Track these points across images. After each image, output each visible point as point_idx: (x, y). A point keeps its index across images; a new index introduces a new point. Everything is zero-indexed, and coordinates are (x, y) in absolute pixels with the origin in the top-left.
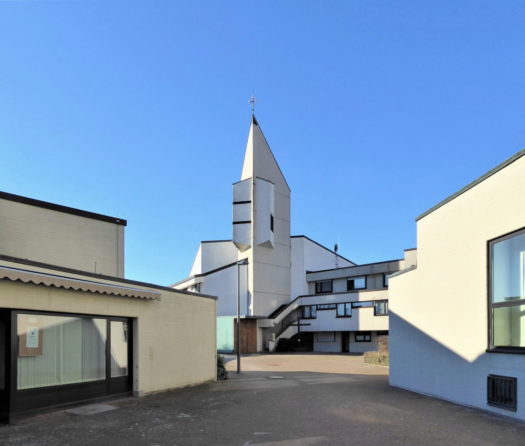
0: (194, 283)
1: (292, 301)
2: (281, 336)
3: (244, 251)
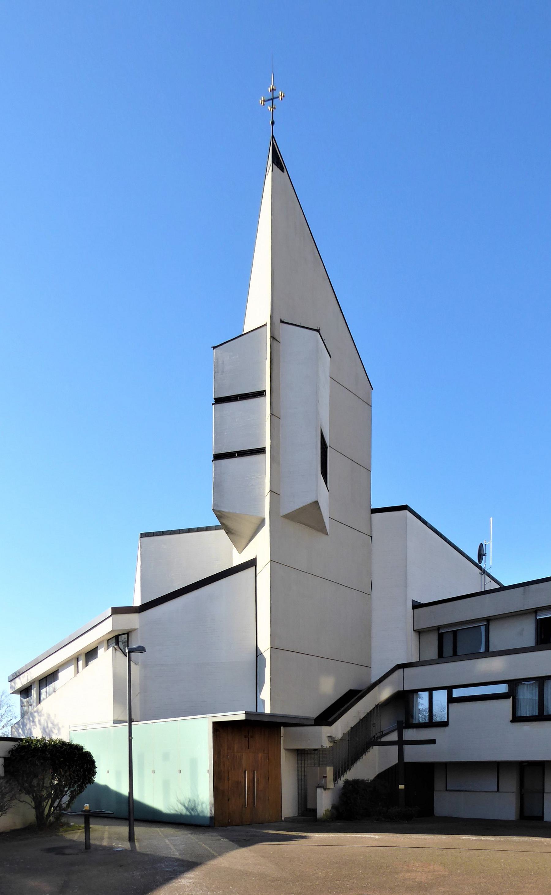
0: (111, 629)
1: (374, 680)
2: (351, 775)
3: (246, 547)
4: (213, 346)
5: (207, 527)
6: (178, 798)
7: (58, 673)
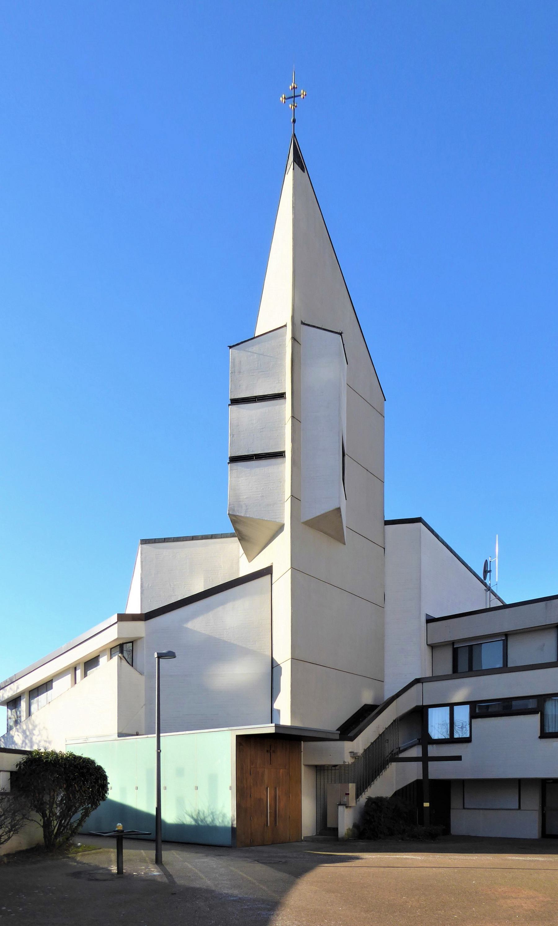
0: (116, 637)
4: (229, 345)
5: (193, 537)
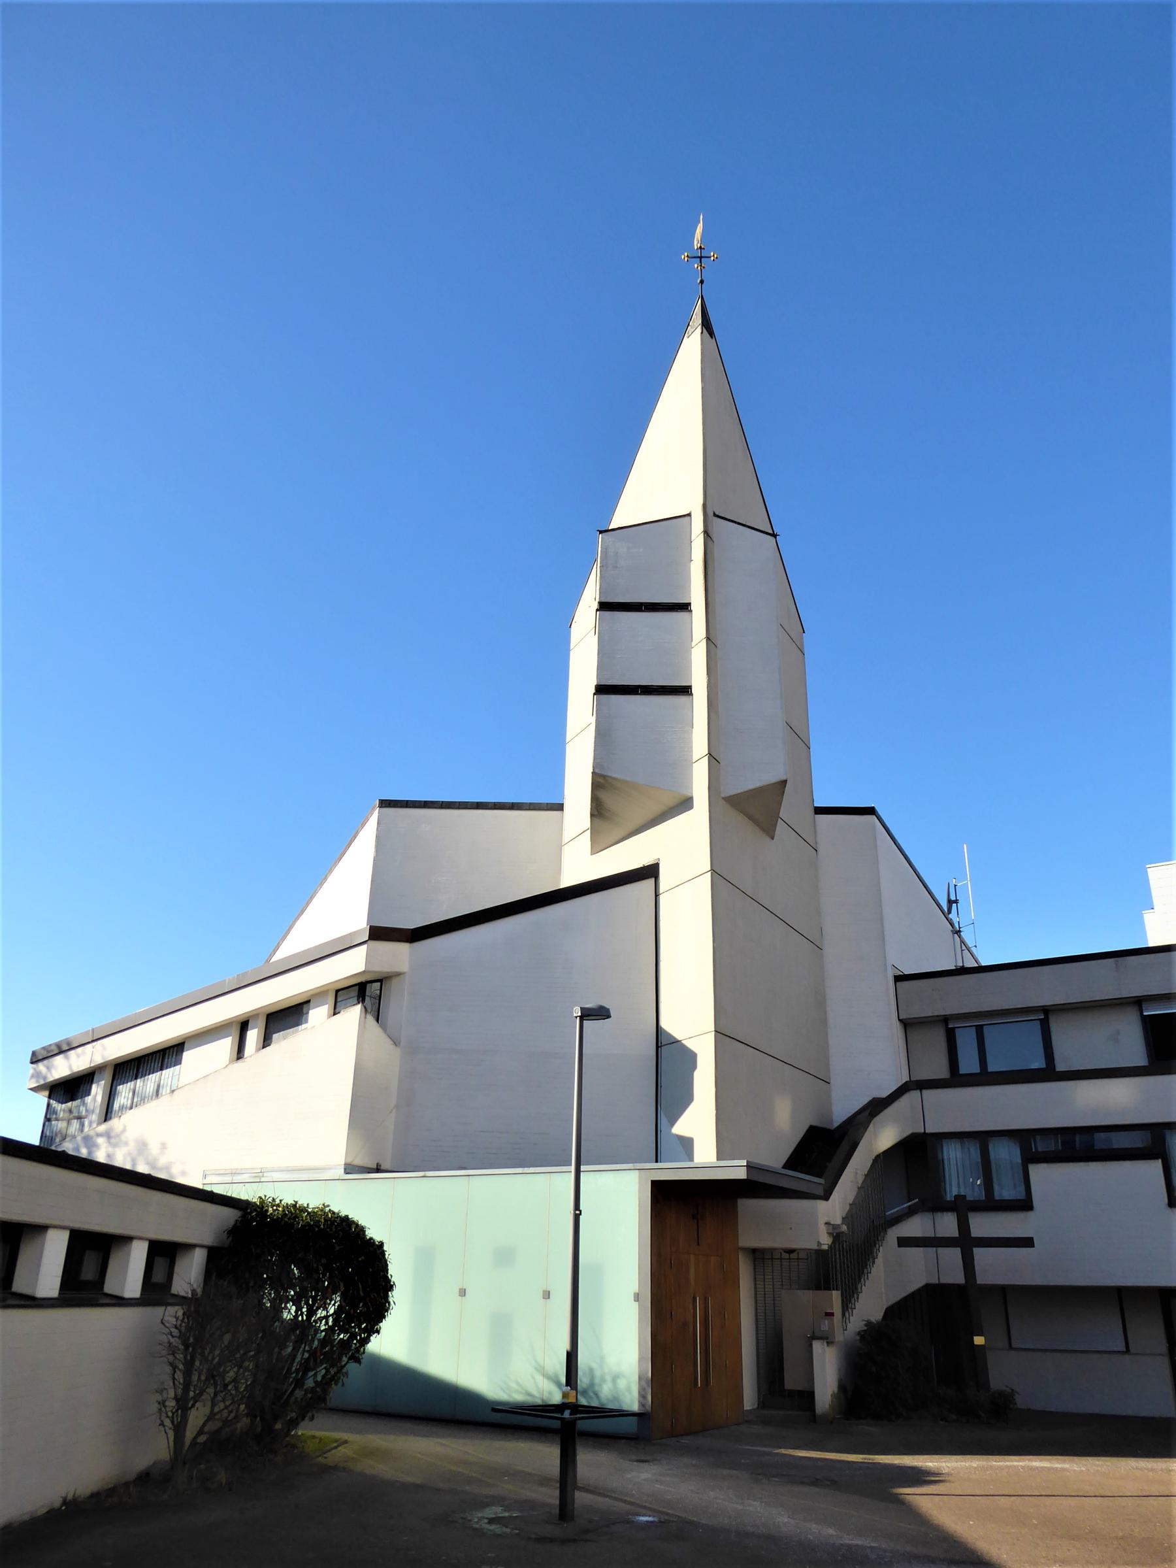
0: (363, 969)
4: (600, 529)
5: (478, 803)
6: (536, 1361)
7: (182, 1051)
